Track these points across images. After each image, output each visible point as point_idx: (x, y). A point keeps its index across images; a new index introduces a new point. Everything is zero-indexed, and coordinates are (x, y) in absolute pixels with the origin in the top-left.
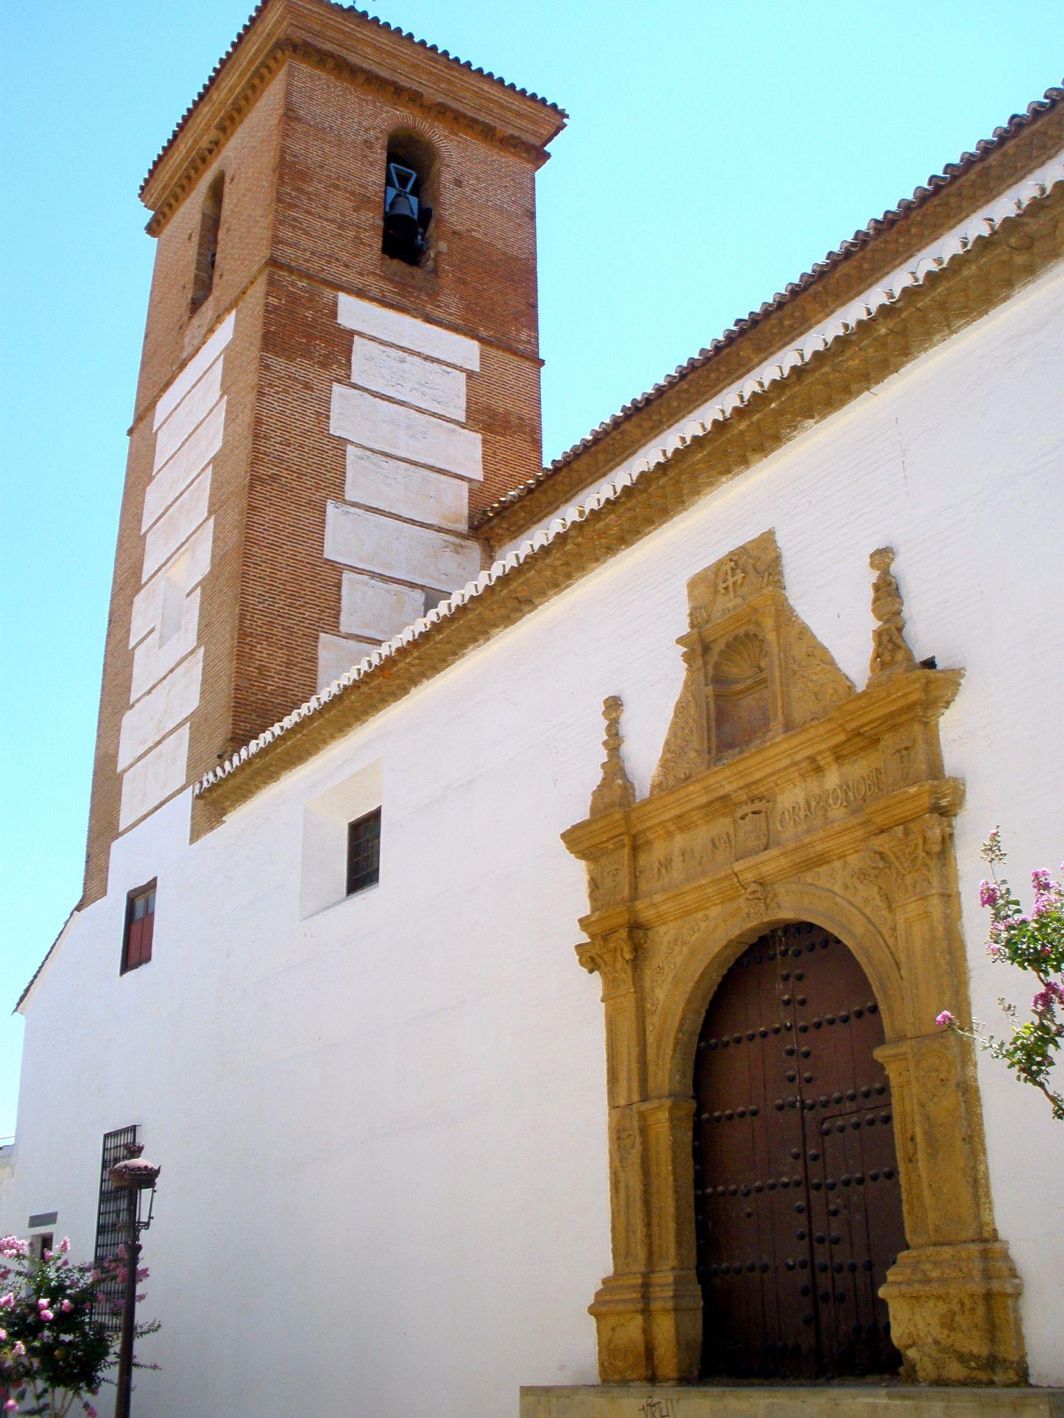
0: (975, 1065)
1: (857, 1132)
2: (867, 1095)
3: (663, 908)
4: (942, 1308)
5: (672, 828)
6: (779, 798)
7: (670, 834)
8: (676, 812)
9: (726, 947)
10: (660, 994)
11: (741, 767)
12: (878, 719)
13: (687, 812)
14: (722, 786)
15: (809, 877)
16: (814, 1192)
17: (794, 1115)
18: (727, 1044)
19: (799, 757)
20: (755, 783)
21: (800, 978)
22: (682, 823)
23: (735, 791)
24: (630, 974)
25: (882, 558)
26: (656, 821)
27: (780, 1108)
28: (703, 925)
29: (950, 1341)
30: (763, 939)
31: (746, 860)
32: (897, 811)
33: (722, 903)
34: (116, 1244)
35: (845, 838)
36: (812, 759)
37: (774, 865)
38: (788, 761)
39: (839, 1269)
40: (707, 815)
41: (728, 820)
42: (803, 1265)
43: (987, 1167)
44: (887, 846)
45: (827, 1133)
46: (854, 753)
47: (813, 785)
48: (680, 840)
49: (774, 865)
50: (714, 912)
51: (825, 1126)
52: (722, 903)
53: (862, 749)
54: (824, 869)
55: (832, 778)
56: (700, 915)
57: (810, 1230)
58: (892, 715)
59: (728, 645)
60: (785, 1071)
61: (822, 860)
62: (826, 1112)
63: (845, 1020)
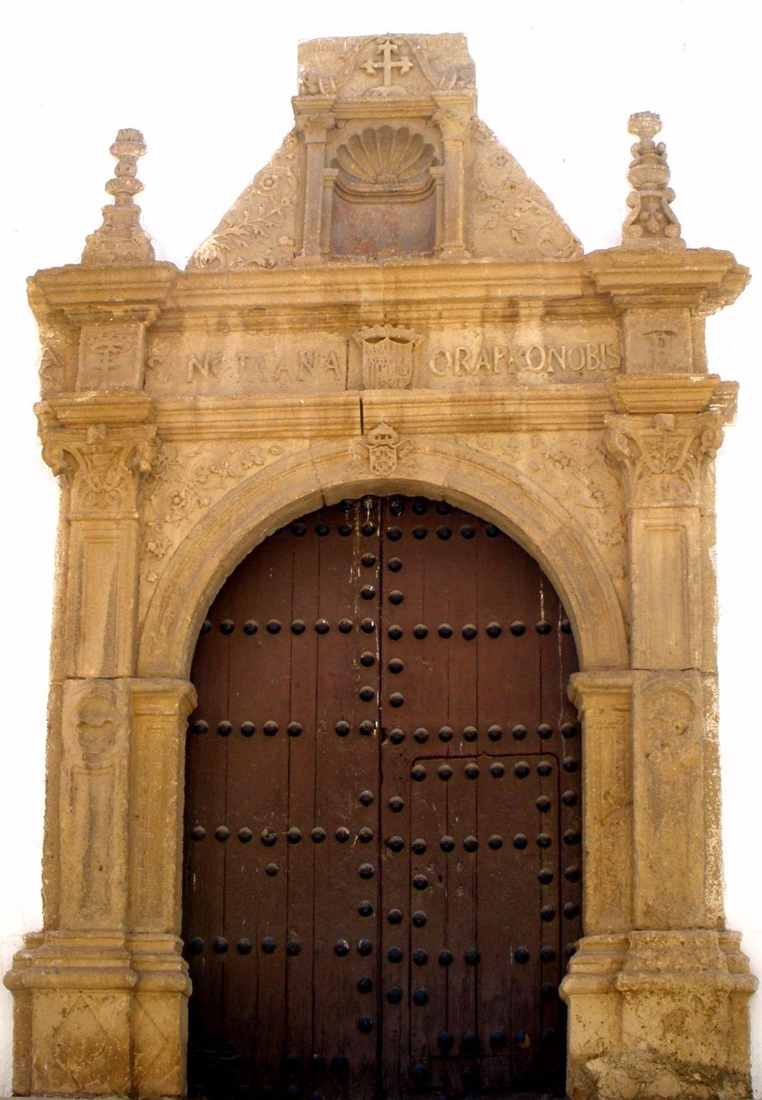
0: (716, 719)
1: (472, 782)
2: (495, 737)
3: (208, 418)
4: (668, 1005)
5: (234, 319)
6: (434, 335)
7: (223, 327)
8: (261, 301)
9: (306, 498)
10: (175, 535)
11: (404, 276)
12: (645, 286)
13: (275, 307)
14: (358, 291)
15: (473, 441)
16: (389, 852)
17: (367, 747)
18: (250, 631)
19: (499, 293)
20: (407, 303)
21: (396, 568)
22: (256, 320)
23: (371, 304)
24: (134, 493)
25: (644, 123)
26: (217, 302)
27: (343, 732)
28: (270, 460)
29: (672, 1049)
30: (343, 506)
31: (389, 392)
32: (663, 397)
33: (312, 438)
34: (377, 312)
35: (556, 408)
36: (512, 302)
37: (431, 411)
38: (481, 293)
39: (422, 961)
40: (303, 320)
41: (335, 339)
42: (365, 951)
43: (719, 842)
44: (641, 433)
45: (419, 777)
46: (573, 316)
47: (497, 336)
48: (235, 342)
49: (431, 411)
50: (295, 446)
51: (419, 767)
52: (312, 438)
53: (586, 315)
54: (500, 439)
55: (530, 335)
56: (267, 445)
57: (380, 902)
58: (665, 289)
59: (370, 133)
60: (360, 684)
61: (506, 425)
62: (425, 750)
63: (470, 636)
